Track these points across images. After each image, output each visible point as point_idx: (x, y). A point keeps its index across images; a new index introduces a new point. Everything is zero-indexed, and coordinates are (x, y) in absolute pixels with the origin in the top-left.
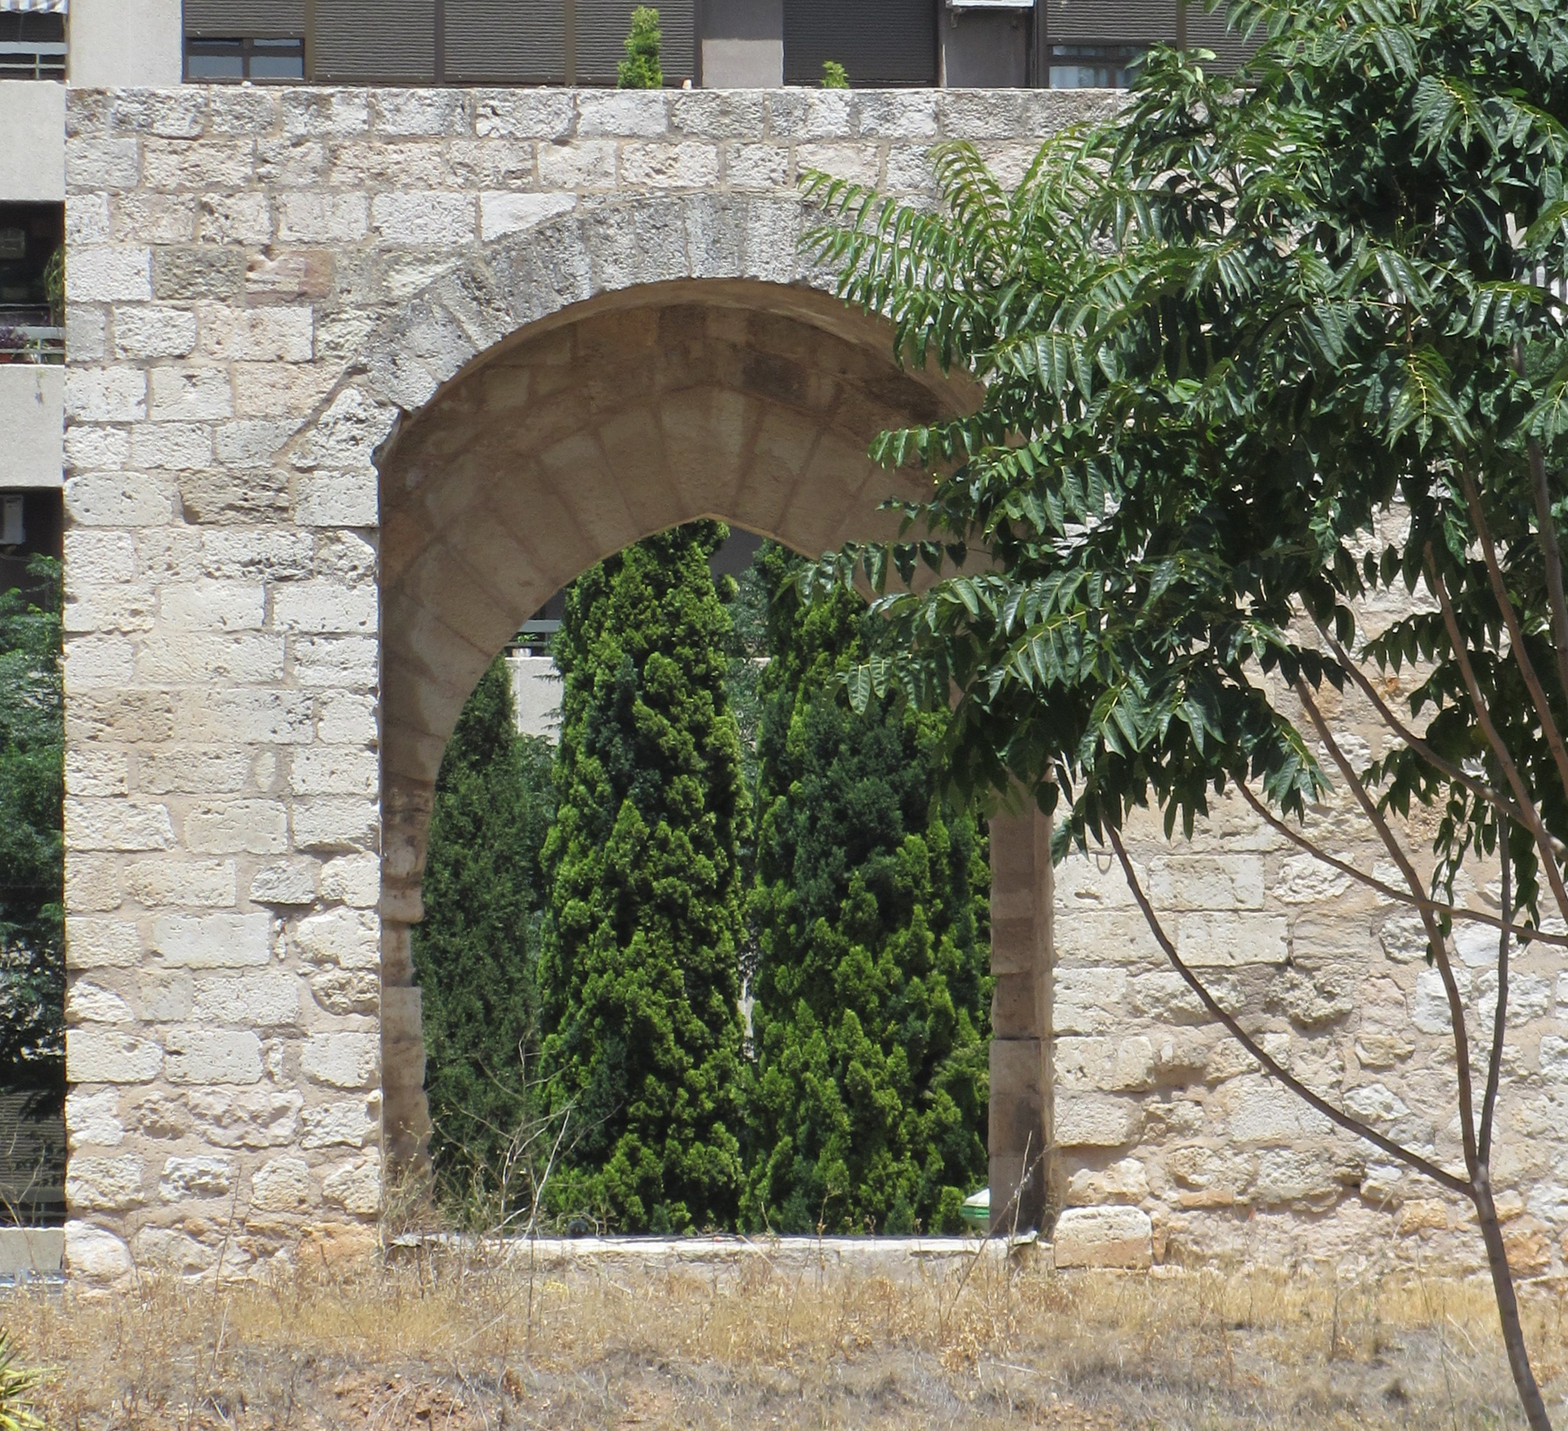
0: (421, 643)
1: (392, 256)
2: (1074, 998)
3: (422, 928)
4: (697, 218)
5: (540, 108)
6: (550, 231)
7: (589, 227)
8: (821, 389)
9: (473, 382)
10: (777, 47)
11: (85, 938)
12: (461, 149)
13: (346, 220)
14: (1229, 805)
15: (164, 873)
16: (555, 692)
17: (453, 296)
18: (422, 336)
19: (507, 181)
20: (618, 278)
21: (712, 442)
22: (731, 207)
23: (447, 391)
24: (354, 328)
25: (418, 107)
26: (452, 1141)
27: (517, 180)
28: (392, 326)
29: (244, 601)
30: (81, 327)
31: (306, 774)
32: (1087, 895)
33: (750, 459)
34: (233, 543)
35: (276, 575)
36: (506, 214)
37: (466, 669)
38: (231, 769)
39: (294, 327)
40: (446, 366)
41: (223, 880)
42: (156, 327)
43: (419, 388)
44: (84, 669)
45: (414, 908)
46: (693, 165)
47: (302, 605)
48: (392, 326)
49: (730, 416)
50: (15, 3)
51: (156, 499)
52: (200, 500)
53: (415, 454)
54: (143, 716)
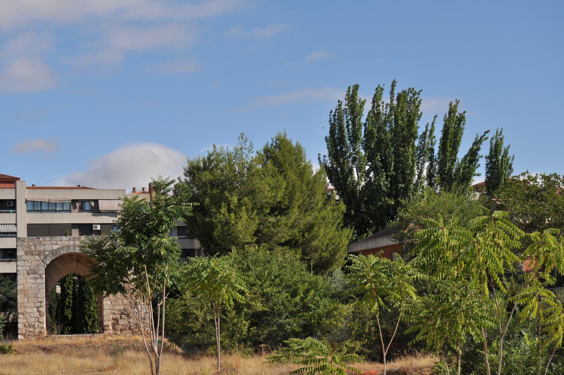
0: (48, 284)
1: (46, 251)
2: (105, 313)
3: (49, 309)
4: (72, 247)
5: (58, 238)
6: (59, 249)
7: (63, 248)
8: (83, 262)
9: (52, 262)
10: (78, 230)
11: (20, 310)
12: (52, 242)
13: (42, 248)
14: (119, 294)
15: (26, 305)
16: (60, 289)
17: (51, 254)
18: (49, 258)
19: (55, 244)
20: (65, 253)
21: (73, 267)
22: (75, 246)
23: (51, 262)
24: (42, 257)
25: (48, 238)
26: (50, 329)
27: (57, 244)
28: (46, 257)
29: (34, 281)
30: (19, 258)
31: (39, 296)
32: (107, 303)
33: (77, 268)
34: (32, 276)
35: (36, 278)
36: (55, 247)
37: (52, 286)
38: (32, 296)
39: (37, 257)
40: (51, 260)
41: (32, 305)
42: (25, 257)
43: (48, 262)
44: (19, 287)
45: (48, 307)
46: (71, 243)
47: (39, 281)
48: (46, 257)
49: (75, 264)
50: (160, 177)
51: (25, 273)
52: (29, 272)
53: (48, 269)
54: (24, 291)
